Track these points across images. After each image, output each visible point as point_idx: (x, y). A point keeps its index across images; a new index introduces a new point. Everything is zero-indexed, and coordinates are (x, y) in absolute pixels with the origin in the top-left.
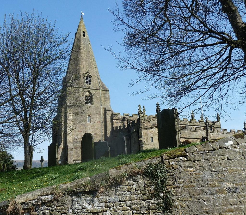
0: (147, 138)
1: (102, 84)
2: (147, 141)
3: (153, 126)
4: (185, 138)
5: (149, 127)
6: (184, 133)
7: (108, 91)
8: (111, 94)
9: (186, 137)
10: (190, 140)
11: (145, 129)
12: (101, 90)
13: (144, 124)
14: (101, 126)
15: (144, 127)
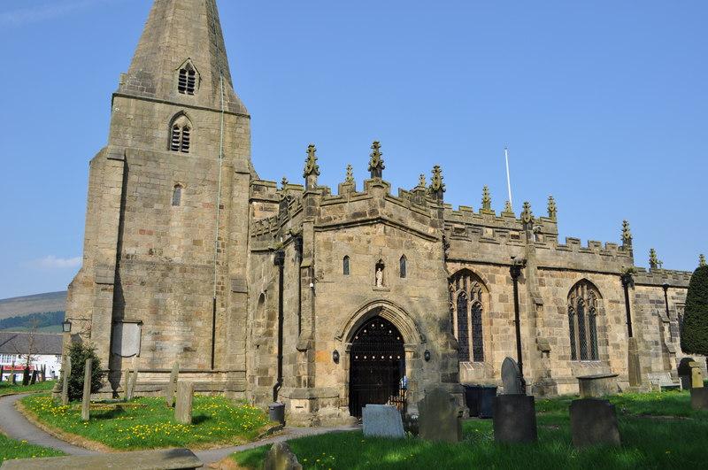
0: (329, 260)
1: (230, 96)
2: (330, 270)
3: (353, 220)
4: (463, 262)
5: (337, 222)
6: (458, 246)
7: (249, 117)
8: (252, 124)
9: (465, 258)
10: (475, 268)
11: (324, 227)
12: (225, 112)
13: (322, 211)
14: (215, 218)
15: (320, 221)
